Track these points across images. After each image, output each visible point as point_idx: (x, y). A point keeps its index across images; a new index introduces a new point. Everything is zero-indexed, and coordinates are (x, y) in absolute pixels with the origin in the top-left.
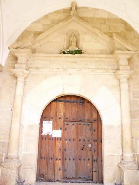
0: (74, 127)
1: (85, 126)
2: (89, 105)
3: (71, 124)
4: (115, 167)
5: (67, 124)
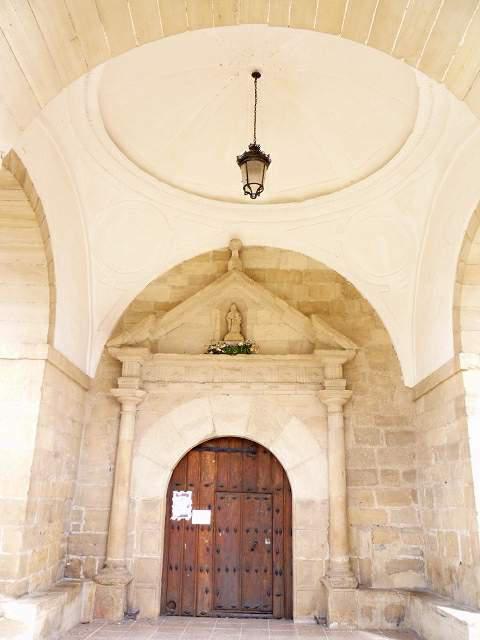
0: (236, 502)
1: (258, 501)
2: (266, 457)
3: (230, 496)
4: (316, 579)
5: (222, 498)
